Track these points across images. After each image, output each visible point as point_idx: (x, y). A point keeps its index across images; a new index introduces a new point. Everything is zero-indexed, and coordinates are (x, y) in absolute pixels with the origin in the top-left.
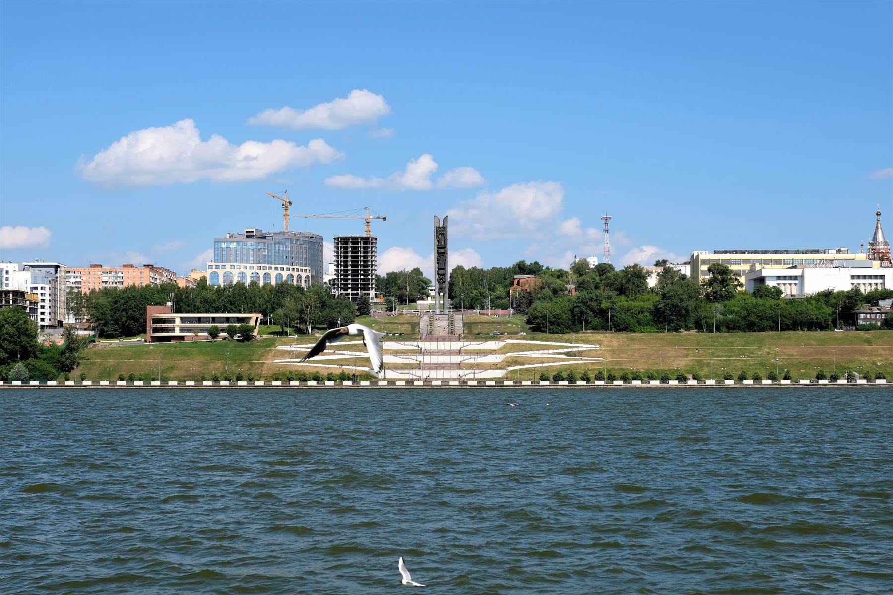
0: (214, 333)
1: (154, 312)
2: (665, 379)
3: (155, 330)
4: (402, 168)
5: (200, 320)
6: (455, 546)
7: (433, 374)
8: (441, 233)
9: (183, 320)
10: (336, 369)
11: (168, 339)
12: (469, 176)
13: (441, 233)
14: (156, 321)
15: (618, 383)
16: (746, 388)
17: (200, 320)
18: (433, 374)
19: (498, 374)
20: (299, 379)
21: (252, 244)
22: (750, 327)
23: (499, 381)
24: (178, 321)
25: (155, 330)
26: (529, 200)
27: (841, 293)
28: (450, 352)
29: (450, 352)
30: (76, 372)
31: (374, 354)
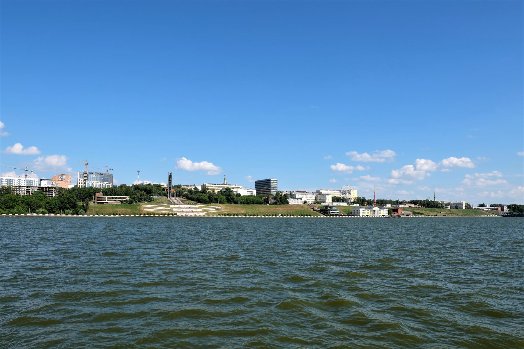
0: (122, 202)
1: (98, 195)
2: (234, 215)
3: (98, 200)
4: (12, 145)
5: (112, 198)
6: (14, 261)
7: (188, 214)
8: (170, 176)
9: (108, 198)
10: (160, 212)
11: (103, 203)
12: (34, 150)
13: (170, 176)
14: (98, 198)
15: (232, 216)
16: (9, 217)
17: (112, 198)
18: (188, 214)
19: (204, 214)
20: (114, 214)
21: (99, 176)
22: (248, 203)
23: (204, 215)
24: (107, 199)
25: (98, 200)
26: (56, 161)
27: (244, 196)
28: (187, 208)
29: (187, 208)
30: (88, 212)
31: (155, 208)
